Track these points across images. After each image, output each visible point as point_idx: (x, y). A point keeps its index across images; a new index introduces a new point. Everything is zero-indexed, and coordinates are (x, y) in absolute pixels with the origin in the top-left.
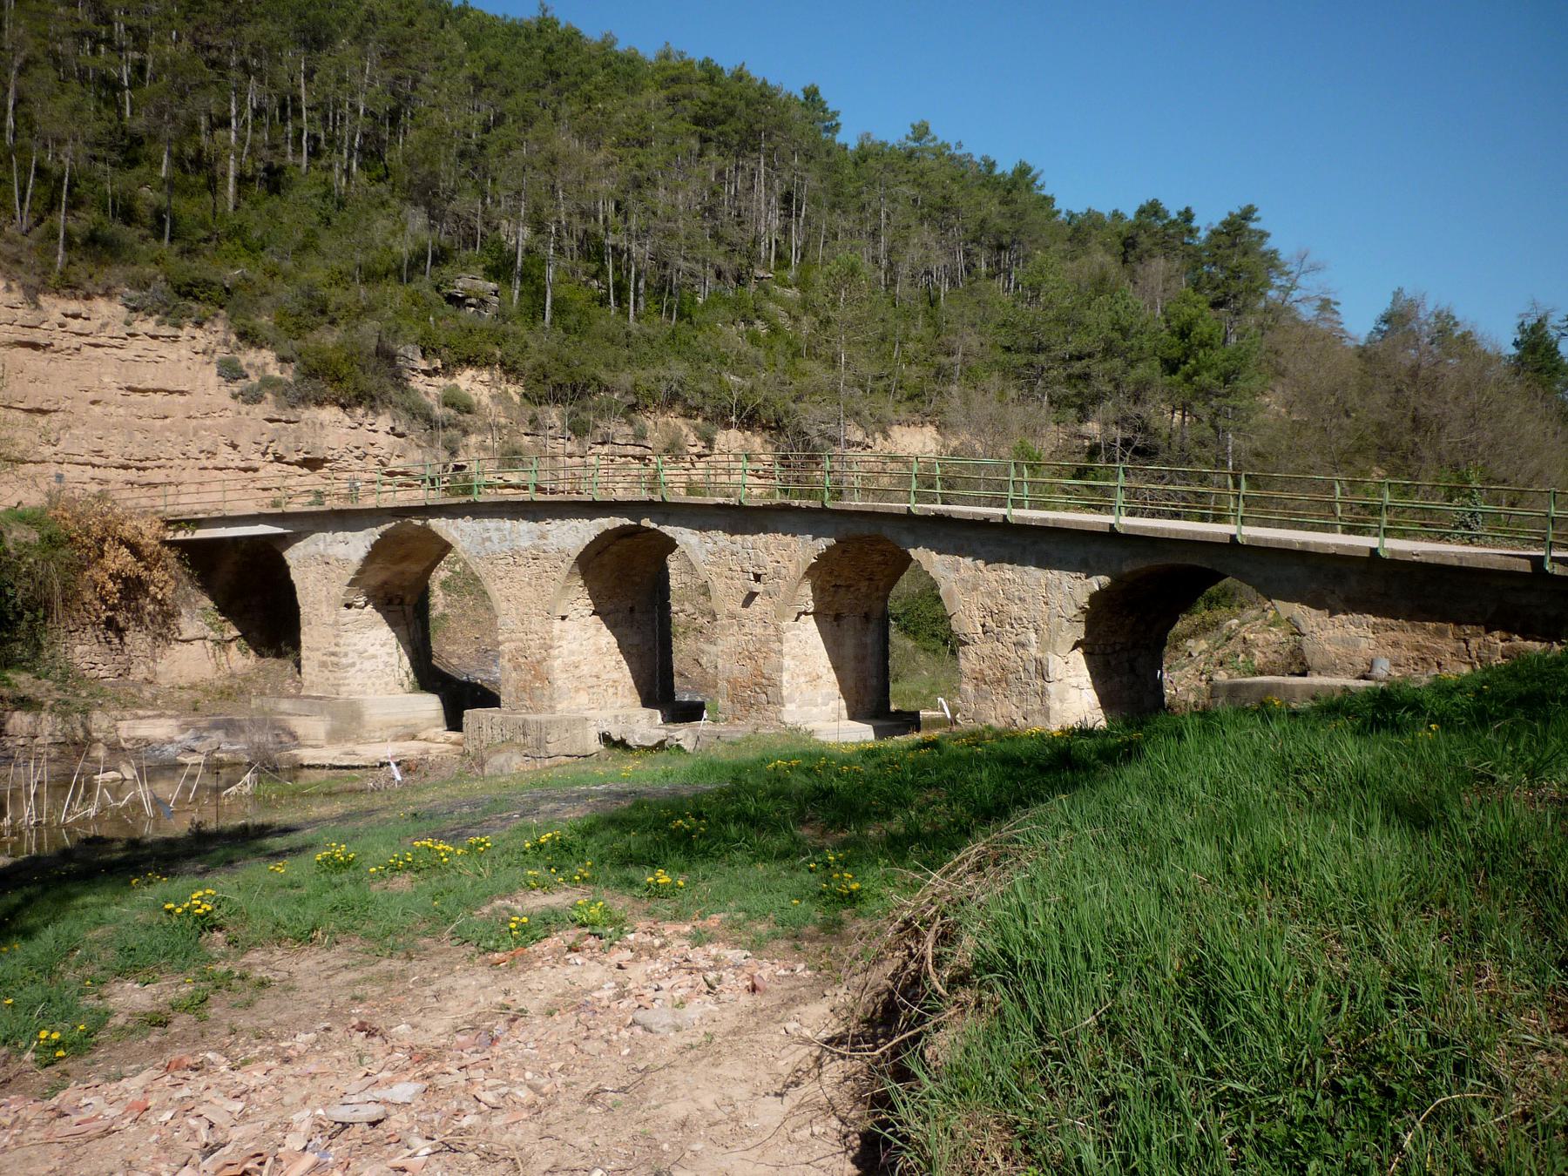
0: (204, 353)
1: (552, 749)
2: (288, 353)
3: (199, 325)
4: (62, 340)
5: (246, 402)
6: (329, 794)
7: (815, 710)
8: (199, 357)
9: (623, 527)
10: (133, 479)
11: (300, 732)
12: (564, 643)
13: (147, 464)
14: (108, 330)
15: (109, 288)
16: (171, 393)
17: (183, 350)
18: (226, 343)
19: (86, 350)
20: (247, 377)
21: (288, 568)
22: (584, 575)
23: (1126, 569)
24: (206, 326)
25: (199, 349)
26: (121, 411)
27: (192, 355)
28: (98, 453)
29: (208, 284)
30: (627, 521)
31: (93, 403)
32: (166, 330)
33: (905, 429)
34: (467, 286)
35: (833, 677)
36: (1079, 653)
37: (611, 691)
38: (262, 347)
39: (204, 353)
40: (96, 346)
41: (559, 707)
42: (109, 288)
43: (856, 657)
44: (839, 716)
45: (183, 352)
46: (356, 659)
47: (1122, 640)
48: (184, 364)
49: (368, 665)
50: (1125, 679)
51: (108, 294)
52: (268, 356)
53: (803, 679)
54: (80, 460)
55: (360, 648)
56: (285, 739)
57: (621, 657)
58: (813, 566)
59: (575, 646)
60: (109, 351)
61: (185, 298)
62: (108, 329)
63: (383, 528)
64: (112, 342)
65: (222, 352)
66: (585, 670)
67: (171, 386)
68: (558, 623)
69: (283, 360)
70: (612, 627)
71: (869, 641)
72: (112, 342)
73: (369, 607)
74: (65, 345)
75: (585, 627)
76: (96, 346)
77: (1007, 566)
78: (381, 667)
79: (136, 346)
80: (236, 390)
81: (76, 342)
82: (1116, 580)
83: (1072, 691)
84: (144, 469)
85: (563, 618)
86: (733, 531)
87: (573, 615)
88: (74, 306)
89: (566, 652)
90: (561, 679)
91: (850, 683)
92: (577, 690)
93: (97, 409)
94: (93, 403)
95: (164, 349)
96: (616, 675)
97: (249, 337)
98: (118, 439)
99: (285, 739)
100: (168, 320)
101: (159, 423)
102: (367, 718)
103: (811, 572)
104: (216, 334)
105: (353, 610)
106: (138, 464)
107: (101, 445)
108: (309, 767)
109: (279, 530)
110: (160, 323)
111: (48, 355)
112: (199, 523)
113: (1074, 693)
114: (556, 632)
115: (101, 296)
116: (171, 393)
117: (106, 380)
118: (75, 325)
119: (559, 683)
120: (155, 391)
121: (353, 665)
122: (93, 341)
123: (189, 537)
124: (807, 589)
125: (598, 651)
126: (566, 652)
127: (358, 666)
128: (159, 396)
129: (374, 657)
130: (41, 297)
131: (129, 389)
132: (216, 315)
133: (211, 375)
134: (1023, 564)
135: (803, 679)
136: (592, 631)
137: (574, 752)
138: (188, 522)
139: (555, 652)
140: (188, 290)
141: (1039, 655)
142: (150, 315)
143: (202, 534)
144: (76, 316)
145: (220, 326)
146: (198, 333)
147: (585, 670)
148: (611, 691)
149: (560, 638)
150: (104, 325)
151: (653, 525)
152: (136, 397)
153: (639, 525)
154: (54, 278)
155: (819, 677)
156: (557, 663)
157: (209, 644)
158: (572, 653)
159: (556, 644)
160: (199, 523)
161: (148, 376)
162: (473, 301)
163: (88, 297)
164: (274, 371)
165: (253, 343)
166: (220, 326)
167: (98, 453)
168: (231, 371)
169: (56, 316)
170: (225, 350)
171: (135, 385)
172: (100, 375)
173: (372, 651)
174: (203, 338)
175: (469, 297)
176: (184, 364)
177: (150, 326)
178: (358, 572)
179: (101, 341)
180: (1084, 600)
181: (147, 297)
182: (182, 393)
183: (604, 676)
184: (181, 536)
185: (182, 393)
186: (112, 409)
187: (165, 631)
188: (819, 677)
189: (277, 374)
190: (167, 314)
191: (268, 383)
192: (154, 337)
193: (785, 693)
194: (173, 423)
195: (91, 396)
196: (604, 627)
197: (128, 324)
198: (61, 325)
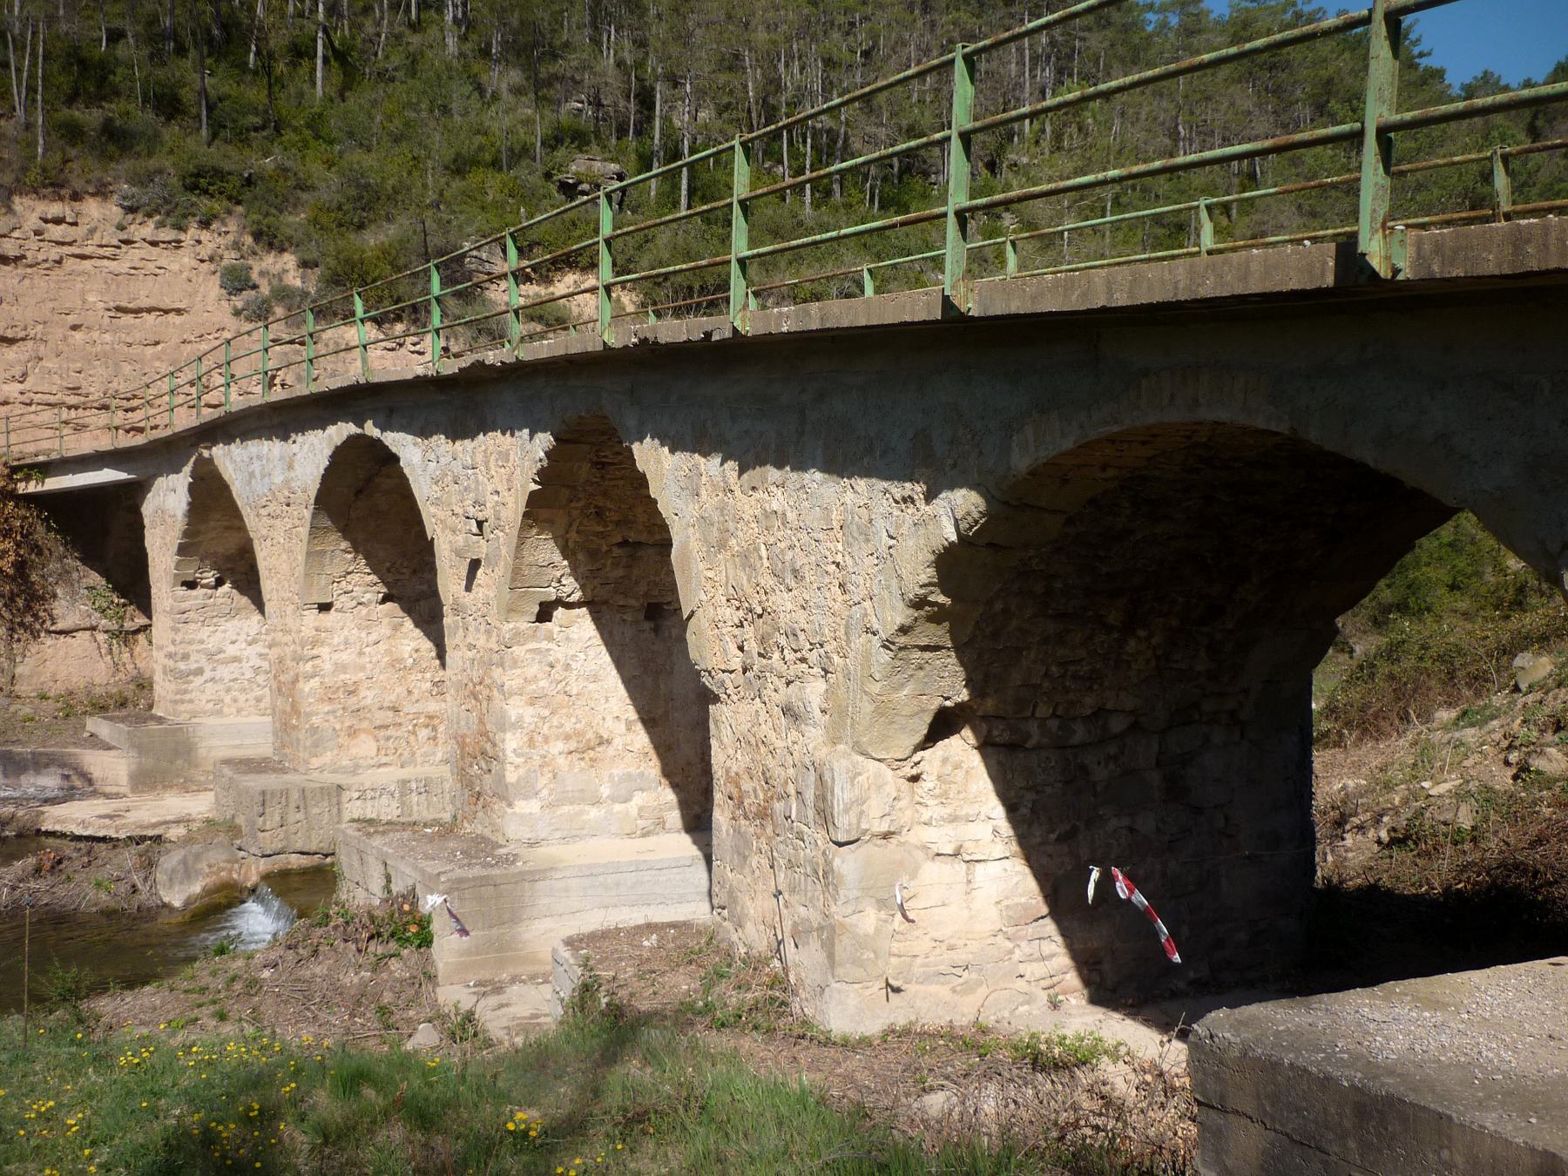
0: (211, 259)
2: (313, 255)
3: (205, 225)
4: (33, 249)
5: (249, 319)
7: (594, 813)
8: (205, 266)
10: (117, 422)
11: (96, 773)
12: (324, 651)
13: (135, 403)
14: (97, 239)
15: (105, 185)
16: (166, 312)
17: (185, 259)
18: (236, 246)
19: (70, 264)
20: (255, 287)
21: (143, 527)
22: (346, 532)
23: (1021, 462)
24: (214, 226)
25: (204, 255)
26: (108, 337)
27: (195, 263)
28: (75, 390)
29: (219, 174)
31: (75, 328)
32: (167, 234)
34: (582, 169)
35: (641, 739)
36: (961, 748)
37: (424, 733)
38: (282, 250)
39: (211, 259)
40: (83, 257)
42: (105, 185)
44: (661, 823)
45: (186, 260)
46: (203, 662)
47: (1129, 702)
48: (185, 275)
49: (225, 672)
50: (1147, 823)
51: (102, 192)
52: (289, 260)
53: (558, 746)
54: (52, 399)
55: (211, 645)
56: (78, 783)
58: (533, 500)
59: (344, 657)
60: (99, 263)
61: (196, 194)
62: (97, 236)
63: (187, 469)
64: (101, 251)
65: (230, 258)
66: (368, 696)
67: (167, 303)
69: (304, 264)
72: (101, 251)
73: (227, 587)
74: (41, 257)
75: (368, 624)
76: (83, 257)
77: (773, 474)
78: (249, 674)
79: (132, 256)
80: (240, 305)
81: (55, 252)
82: (1007, 505)
83: (933, 872)
84: (133, 410)
86: (458, 432)
88: (55, 209)
89: (328, 667)
92: (353, 732)
93: (79, 336)
94: (75, 328)
95: (163, 257)
97: (268, 239)
98: (100, 371)
99: (78, 783)
100: (169, 221)
101: (150, 350)
102: (202, 752)
103: (538, 510)
104: (222, 239)
105: (199, 592)
106: (125, 404)
107: (80, 380)
108: (53, 834)
109: (122, 476)
110: (160, 225)
111: (20, 271)
112: (46, 469)
113: (936, 879)
115: (93, 195)
116: (166, 312)
117: (91, 298)
118: (56, 232)
120: (149, 310)
121: (199, 672)
122: (78, 251)
123: (39, 488)
124: (546, 551)
125: (396, 664)
126: (328, 667)
127: (208, 674)
128: (150, 318)
129: (236, 659)
130: (17, 199)
131: (118, 309)
132: (229, 213)
133: (212, 288)
134: (800, 467)
135: (558, 746)
136: (384, 630)
137: (313, 848)
138: (32, 466)
140: (200, 181)
141: (822, 753)
142: (150, 216)
143: (54, 483)
144: (58, 221)
145: (233, 225)
146: (205, 236)
147: (368, 696)
148: (424, 733)
150: (92, 231)
152: (128, 319)
154: (33, 175)
155: (603, 742)
157: (101, 637)
158: (341, 668)
160: (46, 469)
161: (144, 293)
162: (585, 187)
163: (76, 197)
164: (294, 280)
165: (271, 246)
166: (233, 225)
167: (75, 390)
168: (236, 281)
169: (32, 221)
170: (234, 254)
171: (124, 304)
172: (83, 293)
173: (231, 651)
174: (210, 241)
175: (581, 182)
176: (185, 275)
177: (148, 230)
178: (186, 534)
179: (87, 251)
180: (918, 573)
181: (144, 196)
182: (179, 311)
183: (409, 708)
184: (32, 487)
185: (179, 311)
186: (95, 335)
187: (29, 619)
188: (603, 742)
189: (298, 283)
190: (168, 214)
191: (283, 294)
192: (154, 244)
193: (511, 776)
194: (163, 351)
195: (72, 319)
196: (409, 623)
197: (121, 228)
198: (37, 233)
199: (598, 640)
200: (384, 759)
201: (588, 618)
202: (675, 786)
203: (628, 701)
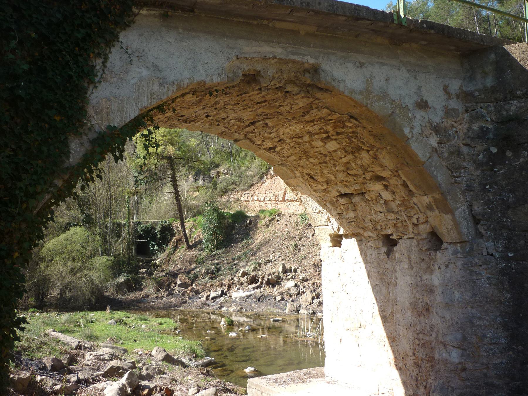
43: (414, 305)
71: (436, 279)
91: (405, 345)
199: (360, 259)
201: (356, 243)
202: (399, 369)
203: (375, 301)
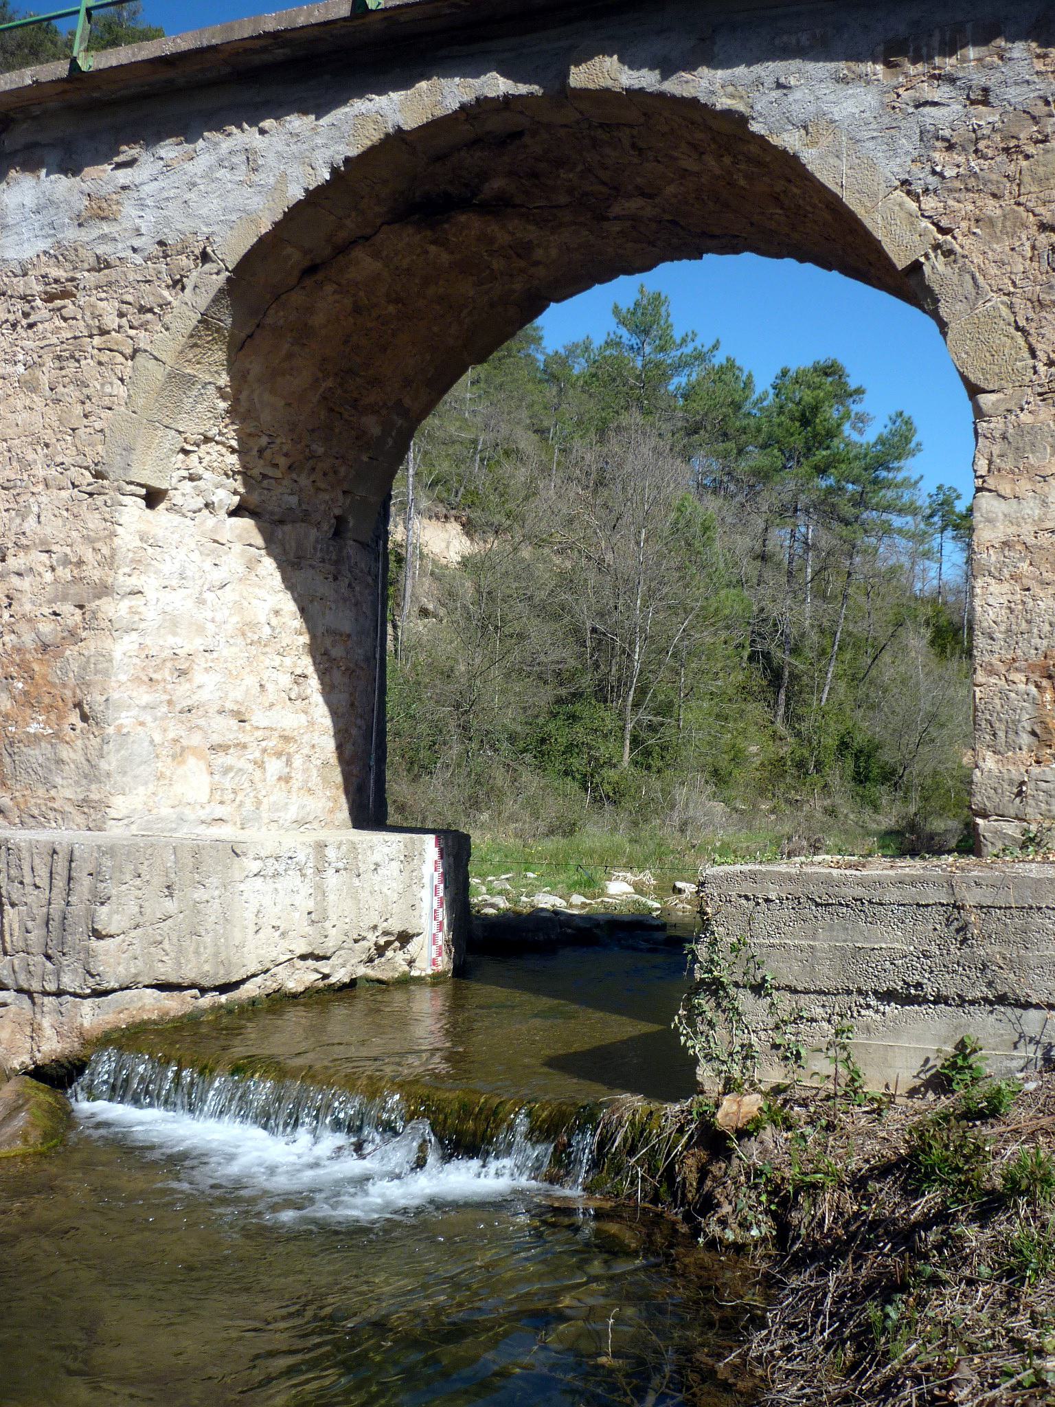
1: (112, 961)
6: (70, 879)
9: (479, 108)
12: (148, 583)
22: (238, 349)
30: (497, 85)
33: (426, 521)
37: (275, 766)
41: (120, 805)
57: (306, 664)
59: (180, 601)
68: (133, 510)
70: (292, 566)
85: (153, 498)
87: (184, 494)
90: (130, 707)
92: (180, 753)
96: (290, 720)
114: (126, 539)
119: (126, 719)
126: (150, 613)
136: (233, 560)
137: (189, 973)
139: (111, 608)
149: (137, 565)
151: (646, 79)
153: (562, 94)
156: (122, 648)
158: (172, 622)
159: (123, 580)
183: (259, 718)
200: (220, 812)
